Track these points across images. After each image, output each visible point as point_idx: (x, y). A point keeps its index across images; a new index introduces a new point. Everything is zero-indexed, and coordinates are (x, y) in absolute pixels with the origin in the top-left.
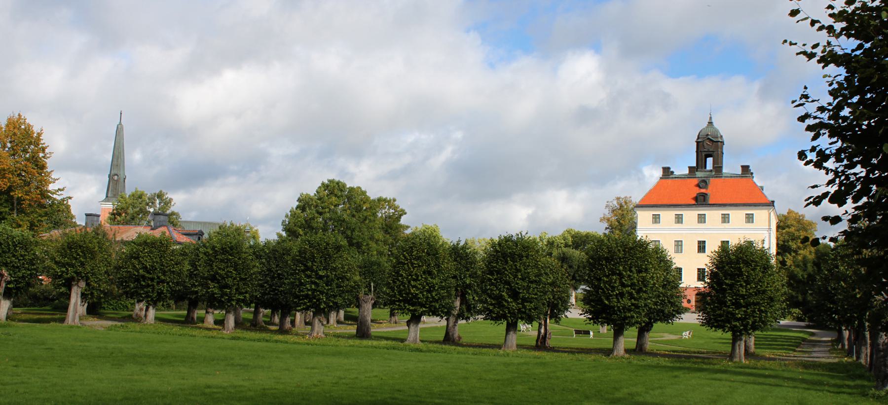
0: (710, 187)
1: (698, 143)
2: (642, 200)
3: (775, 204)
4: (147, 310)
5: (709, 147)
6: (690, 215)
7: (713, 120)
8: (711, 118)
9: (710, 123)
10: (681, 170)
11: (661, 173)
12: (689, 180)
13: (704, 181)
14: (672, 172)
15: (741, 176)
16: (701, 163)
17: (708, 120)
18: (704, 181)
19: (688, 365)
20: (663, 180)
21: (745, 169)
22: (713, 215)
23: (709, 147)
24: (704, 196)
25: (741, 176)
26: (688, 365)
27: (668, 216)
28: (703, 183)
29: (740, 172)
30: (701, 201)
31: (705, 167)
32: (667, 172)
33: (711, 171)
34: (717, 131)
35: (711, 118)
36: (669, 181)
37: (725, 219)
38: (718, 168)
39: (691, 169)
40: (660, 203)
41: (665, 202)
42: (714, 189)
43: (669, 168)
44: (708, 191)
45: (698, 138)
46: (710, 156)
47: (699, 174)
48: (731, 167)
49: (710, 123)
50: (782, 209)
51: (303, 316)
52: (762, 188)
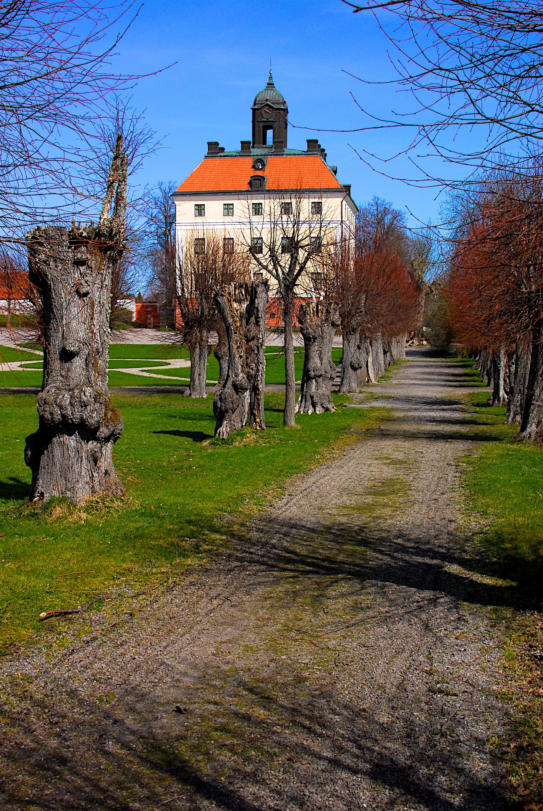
0: (267, 168)
1: (254, 110)
2: (182, 187)
3: (205, 150)
5: (269, 119)
7: (274, 81)
8: (271, 78)
9: (270, 85)
10: (232, 146)
12: (242, 159)
13: (260, 161)
14: (223, 149)
15: (306, 153)
16: (259, 137)
18: (260, 161)
19: (178, 388)
20: (209, 160)
23: (269, 119)
24: (262, 179)
25: (306, 153)
26: (178, 388)
27: (214, 207)
28: (259, 163)
29: (304, 147)
30: (257, 186)
31: (265, 142)
32: (214, 149)
33: (271, 147)
34: (280, 95)
35: (271, 78)
36: (217, 161)
38: (280, 143)
39: (244, 144)
40: (204, 190)
41: (210, 189)
43: (217, 144)
44: (266, 174)
45: (255, 104)
46: (270, 127)
47: (255, 151)
48: (296, 141)
49: (270, 85)
50: (362, 197)
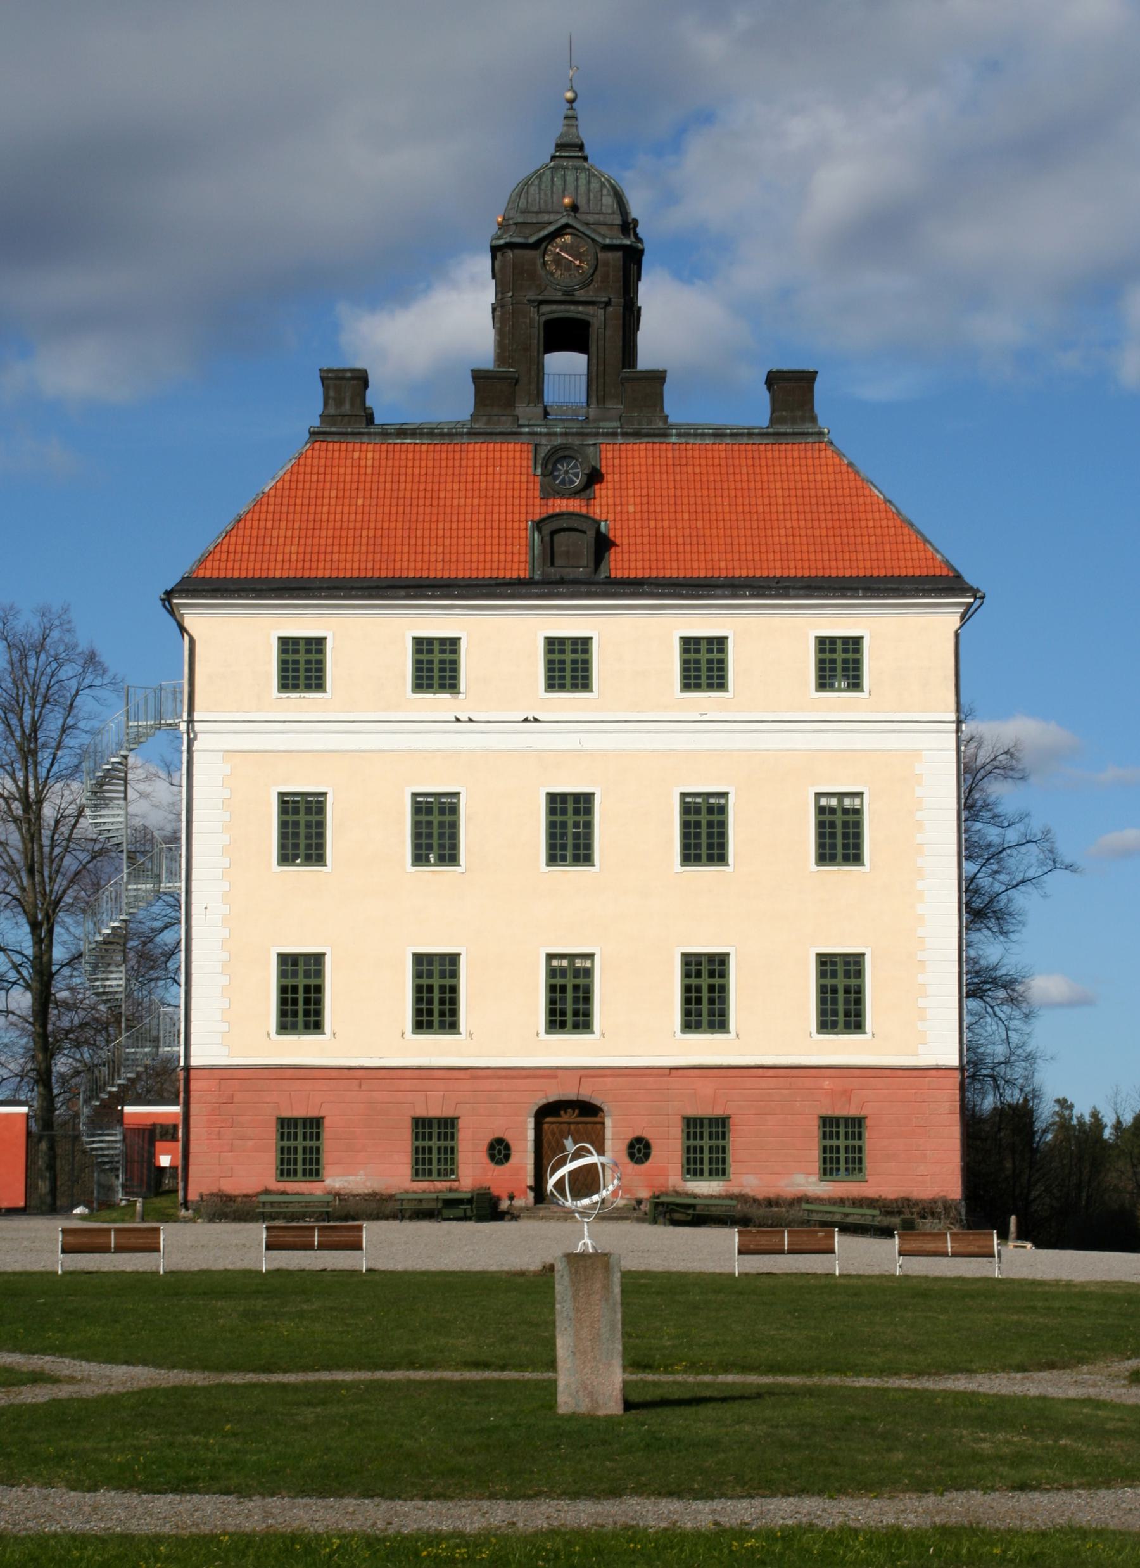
4: (1035, 1199)
6: (502, 641)
8: (571, 118)
9: (570, 149)
11: (316, 406)
17: (556, 131)
21: (792, 391)
22: (635, 640)
23: (572, 279)
25: (771, 435)
27: (370, 642)
28: (567, 465)
30: (574, 561)
37: (704, 666)
40: (323, 571)
41: (351, 569)
42: (630, 495)
44: (603, 506)
49: (570, 149)
51: (947, 1205)
52: (264, 1498)
